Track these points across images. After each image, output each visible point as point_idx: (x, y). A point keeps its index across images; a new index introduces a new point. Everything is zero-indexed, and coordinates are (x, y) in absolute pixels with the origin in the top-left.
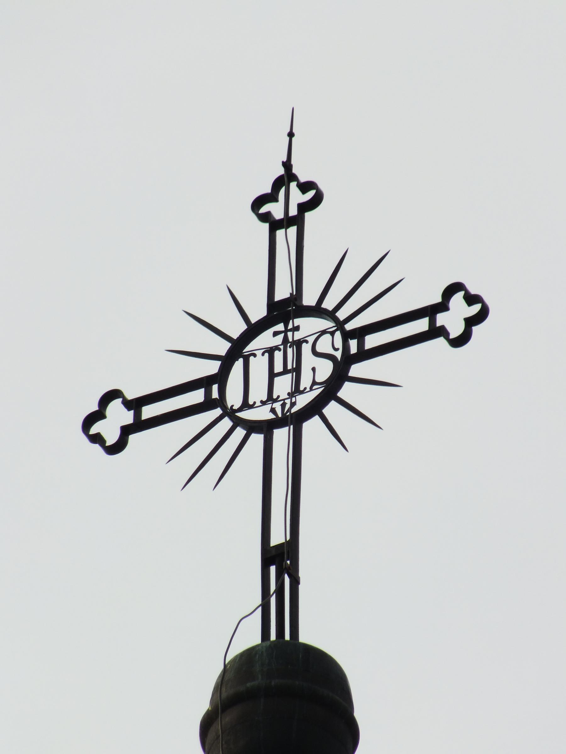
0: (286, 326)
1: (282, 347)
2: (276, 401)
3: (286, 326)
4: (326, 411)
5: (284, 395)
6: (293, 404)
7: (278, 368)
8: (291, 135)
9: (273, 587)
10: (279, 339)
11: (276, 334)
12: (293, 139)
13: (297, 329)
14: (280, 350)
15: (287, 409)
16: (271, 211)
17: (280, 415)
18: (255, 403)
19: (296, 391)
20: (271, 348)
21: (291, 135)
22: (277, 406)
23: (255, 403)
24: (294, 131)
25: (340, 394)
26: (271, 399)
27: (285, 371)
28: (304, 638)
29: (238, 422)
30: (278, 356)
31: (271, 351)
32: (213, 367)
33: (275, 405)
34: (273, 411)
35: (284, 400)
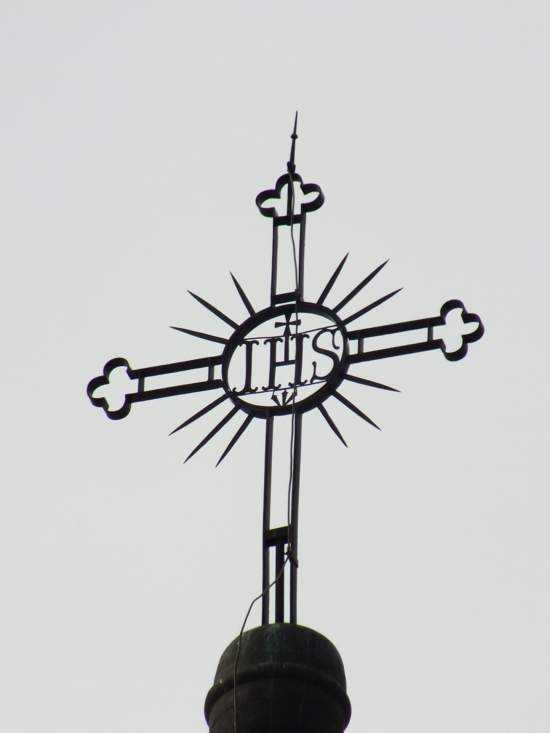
0: (288, 318)
1: (284, 338)
2: (277, 389)
3: (288, 318)
6: (295, 394)
7: (280, 358)
8: (294, 137)
11: (278, 325)
12: (296, 140)
14: (281, 341)
18: (257, 388)
19: (298, 382)
20: (273, 338)
21: (294, 137)
22: (279, 394)
23: (257, 388)
24: (297, 133)
26: (272, 386)
27: (287, 362)
29: (240, 405)
30: (280, 346)
31: (273, 341)
32: (218, 350)
34: (274, 398)
35: (285, 389)
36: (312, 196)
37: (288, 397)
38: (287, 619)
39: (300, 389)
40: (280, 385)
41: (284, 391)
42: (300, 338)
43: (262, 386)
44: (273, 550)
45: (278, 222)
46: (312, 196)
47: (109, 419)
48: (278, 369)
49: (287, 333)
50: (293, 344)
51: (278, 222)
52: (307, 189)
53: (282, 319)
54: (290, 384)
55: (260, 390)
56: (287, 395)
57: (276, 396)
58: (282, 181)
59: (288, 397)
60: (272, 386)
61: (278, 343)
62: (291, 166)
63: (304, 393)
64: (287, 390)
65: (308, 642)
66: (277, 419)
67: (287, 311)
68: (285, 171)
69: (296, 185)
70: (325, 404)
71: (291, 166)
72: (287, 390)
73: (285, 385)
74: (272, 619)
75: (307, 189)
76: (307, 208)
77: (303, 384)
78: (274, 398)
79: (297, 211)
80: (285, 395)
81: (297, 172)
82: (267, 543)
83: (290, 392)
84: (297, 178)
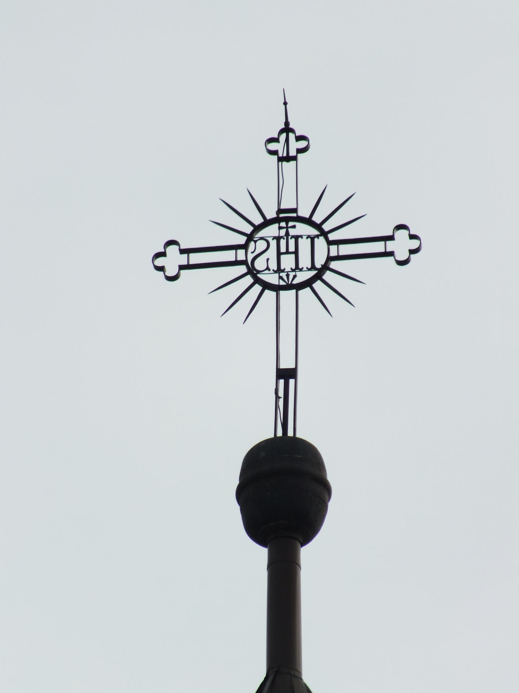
0: (287, 224)
1: (285, 237)
2: (283, 271)
3: (287, 224)
4: (315, 285)
5: (288, 269)
6: (295, 276)
7: (283, 249)
8: (285, 103)
9: (281, 394)
10: (283, 232)
11: (280, 228)
12: (287, 106)
13: (294, 227)
14: (284, 239)
15: (286, 278)
16: (279, 151)
17: (290, 283)
18: (303, 268)
19: (297, 268)
20: (297, 236)
21: (285, 103)
22: (283, 275)
23: (303, 268)
24: (287, 101)
25: (324, 277)
26: (279, 270)
27: (287, 252)
28: (298, 435)
29: (257, 281)
30: (283, 242)
31: (278, 239)
33: (281, 274)
34: (281, 278)
35: (288, 272)
36: (302, 144)
37: (285, 278)
38: (290, 434)
39: (298, 274)
40: (284, 269)
41: (286, 273)
42: (297, 238)
43: (303, 267)
44: (282, 382)
45: (281, 159)
46: (302, 144)
47: (167, 281)
48: (282, 257)
49: (287, 234)
50: (292, 242)
51: (281, 159)
52: (299, 138)
53: (283, 224)
54: (291, 269)
55: (305, 269)
56: (289, 276)
57: (289, 274)
58: (281, 131)
59: (285, 278)
60: (279, 270)
61: (282, 240)
62: (287, 123)
63: (302, 277)
64: (289, 273)
65: (295, 456)
66: (283, 294)
67: (287, 220)
68: (283, 126)
69: (292, 136)
70: (315, 285)
71: (287, 123)
72: (289, 273)
73: (288, 269)
74: (280, 434)
75: (299, 138)
76: (300, 151)
77: (301, 270)
78: (281, 278)
79: (293, 153)
80: (288, 276)
81: (291, 126)
82: (278, 377)
83: (292, 275)
84: (293, 131)
